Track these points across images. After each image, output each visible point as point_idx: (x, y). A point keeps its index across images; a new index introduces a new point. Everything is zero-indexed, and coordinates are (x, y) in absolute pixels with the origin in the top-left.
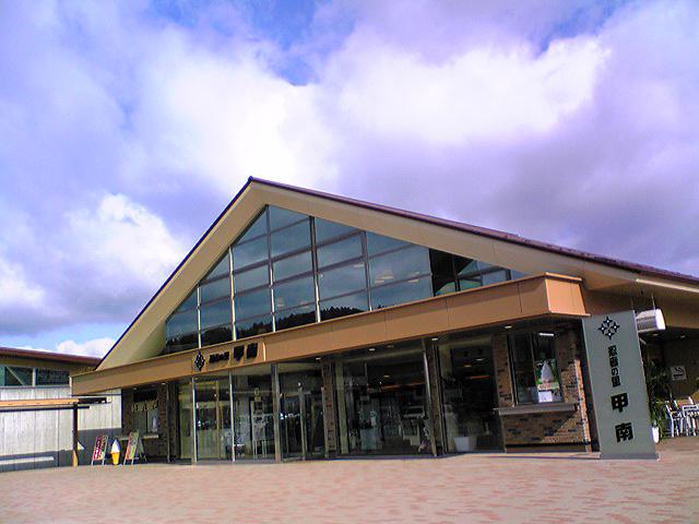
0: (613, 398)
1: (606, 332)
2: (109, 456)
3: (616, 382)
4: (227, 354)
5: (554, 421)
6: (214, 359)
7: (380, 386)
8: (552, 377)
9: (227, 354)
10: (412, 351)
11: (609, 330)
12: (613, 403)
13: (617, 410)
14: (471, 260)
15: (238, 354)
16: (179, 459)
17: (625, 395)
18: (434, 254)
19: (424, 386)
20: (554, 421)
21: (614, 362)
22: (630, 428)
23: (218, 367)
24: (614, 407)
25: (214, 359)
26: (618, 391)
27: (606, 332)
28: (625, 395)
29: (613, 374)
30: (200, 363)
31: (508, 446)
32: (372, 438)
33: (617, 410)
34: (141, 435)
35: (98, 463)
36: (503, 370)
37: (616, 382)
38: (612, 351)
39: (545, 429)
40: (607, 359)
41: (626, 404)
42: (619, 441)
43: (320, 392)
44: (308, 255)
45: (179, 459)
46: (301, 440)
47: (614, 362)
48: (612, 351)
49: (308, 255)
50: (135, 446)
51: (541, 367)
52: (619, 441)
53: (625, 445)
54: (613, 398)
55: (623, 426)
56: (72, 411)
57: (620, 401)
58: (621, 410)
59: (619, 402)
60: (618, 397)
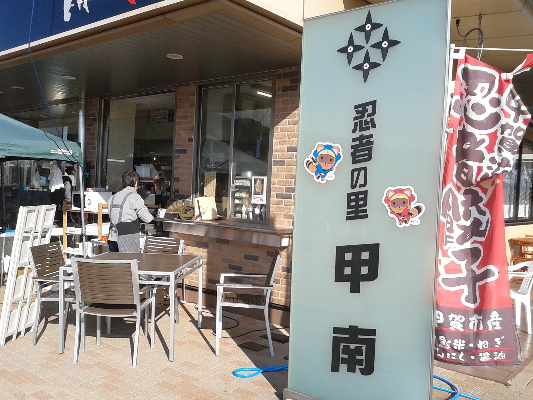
0: (341, 251)
5: (247, 257)
10: (33, 44)
12: (340, 263)
13: (347, 285)
17: (374, 249)
19: (84, 172)
20: (247, 257)
22: (371, 345)
24: (340, 277)
26: (358, 233)
28: (374, 249)
33: (347, 285)
36: (185, 151)
38: (365, 115)
41: (373, 275)
42: (335, 368)
47: (362, 150)
48: (365, 115)
52: (335, 368)
54: (341, 251)
55: (353, 332)
56: (282, 303)
57: (356, 263)
58: (355, 289)
59: (357, 266)
60: (356, 249)
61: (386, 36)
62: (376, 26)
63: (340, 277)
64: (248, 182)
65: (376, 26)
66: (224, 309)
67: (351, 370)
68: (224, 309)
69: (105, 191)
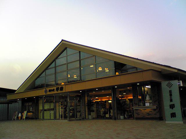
0: (170, 105)
1: (169, 86)
2: (18, 117)
3: (171, 101)
4: (54, 89)
6: (50, 91)
7: (95, 100)
8: (149, 99)
9: (54, 89)
11: (170, 85)
14: (125, 65)
15: (57, 89)
16: (44, 119)
17: (174, 104)
18: (115, 62)
21: (171, 95)
22: (175, 115)
23: (52, 93)
24: (170, 108)
25: (50, 91)
26: (172, 103)
27: (169, 86)
28: (174, 104)
29: (170, 98)
30: (46, 91)
31: (136, 118)
32: (94, 114)
34: (27, 112)
35: (14, 120)
36: (135, 96)
37: (171, 101)
38: (170, 92)
39: (147, 113)
40: (168, 94)
41: (174, 107)
42: (171, 117)
43: (80, 101)
44: (66, 66)
45: (38, 119)
46: (71, 115)
47: (171, 95)
48: (170, 92)
49: (66, 66)
50: (19, 116)
51: (146, 96)
53: (173, 118)
57: (172, 106)
58: (172, 109)
59: (172, 106)
60: (172, 105)
61: (168, 86)
62: (170, 83)
63: (170, 108)
64: (59, 118)
65: (170, 83)
66: (59, 87)
67: (173, 117)
68: (59, 87)
69: (55, 118)
